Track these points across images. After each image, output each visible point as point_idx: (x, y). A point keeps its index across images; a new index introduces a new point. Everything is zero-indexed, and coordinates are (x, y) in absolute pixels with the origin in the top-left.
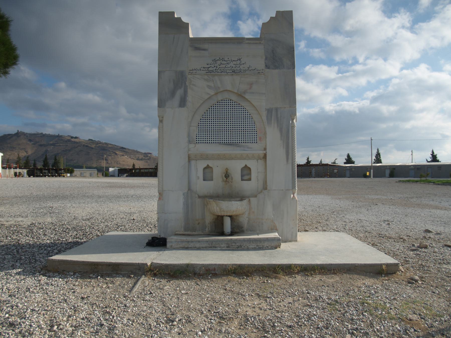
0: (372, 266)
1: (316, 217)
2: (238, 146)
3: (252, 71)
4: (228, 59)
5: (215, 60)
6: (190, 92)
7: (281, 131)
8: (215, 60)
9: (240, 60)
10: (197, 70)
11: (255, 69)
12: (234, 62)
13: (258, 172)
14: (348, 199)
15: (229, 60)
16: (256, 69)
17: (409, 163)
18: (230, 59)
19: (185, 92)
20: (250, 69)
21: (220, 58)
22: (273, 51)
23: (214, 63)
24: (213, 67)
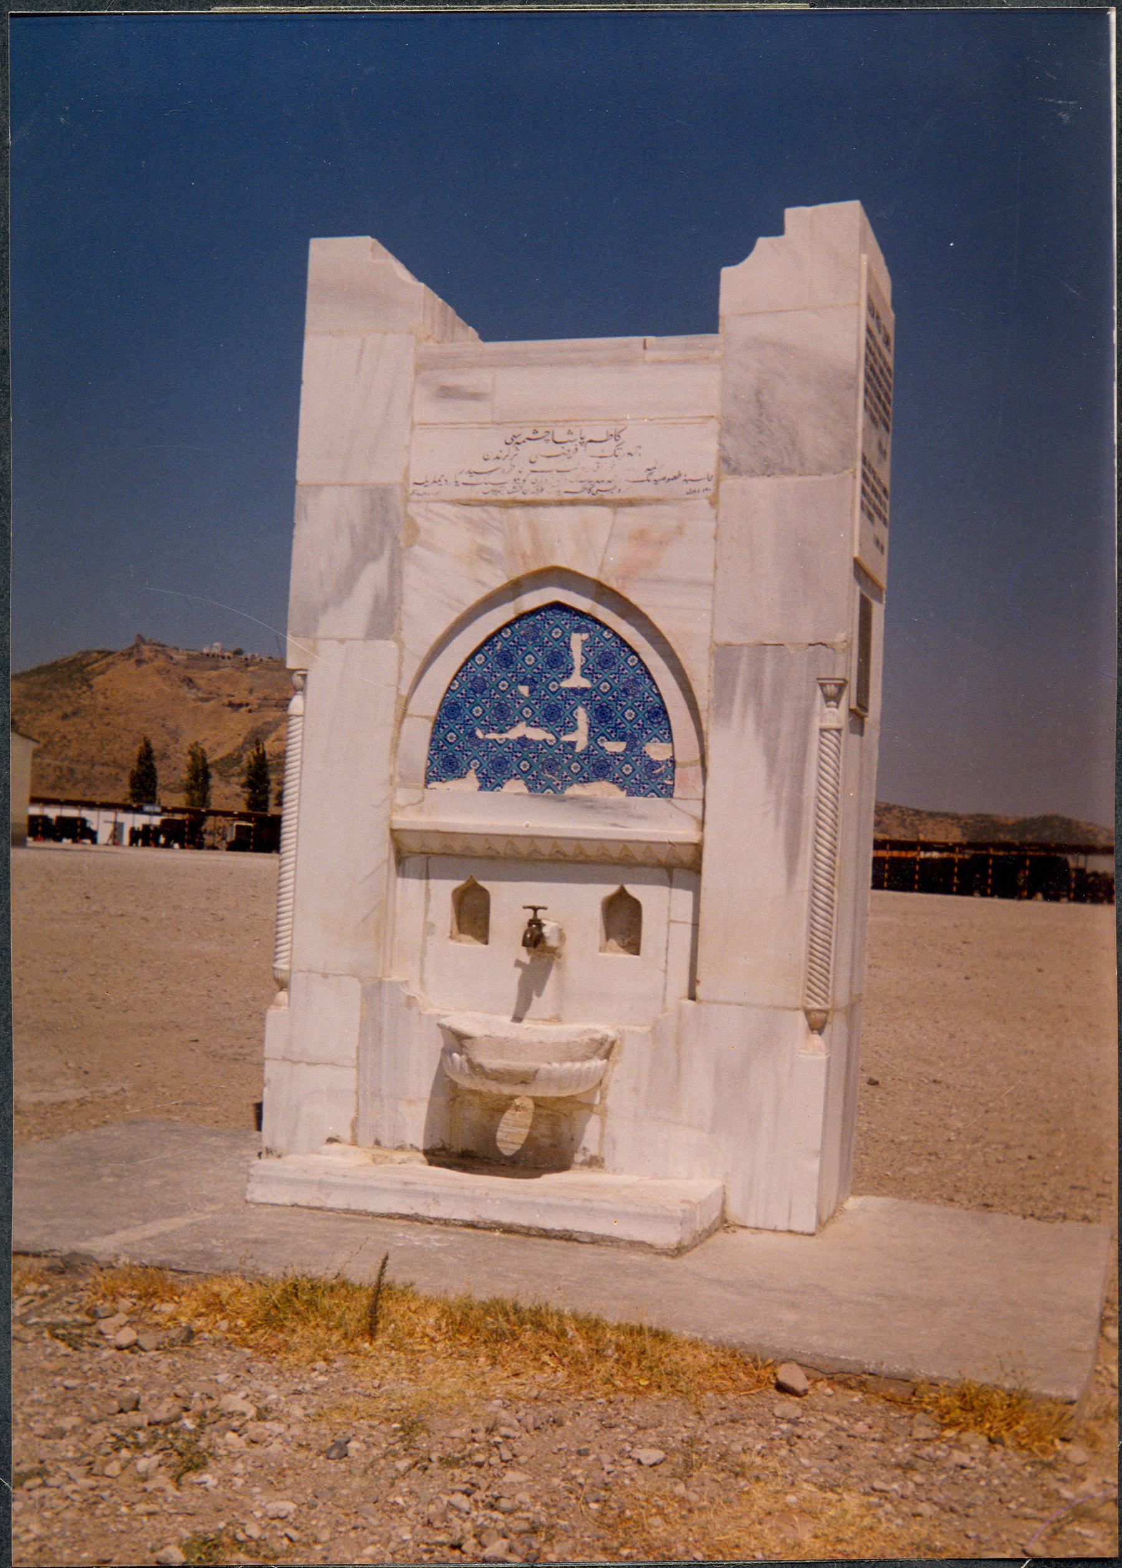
0: (390, 20)
1: (229, 1500)
2: (591, 807)
3: (663, 482)
4: (570, 432)
5: (516, 440)
6: (412, 575)
7: (771, 754)
8: (516, 440)
9: (617, 436)
10: (443, 482)
11: (675, 478)
12: (596, 449)
13: (670, 921)
14: (63, 1272)
15: (571, 438)
16: (682, 478)
17: (591, 1212)
18: (576, 435)
19: (395, 574)
20: (657, 475)
21: (536, 432)
22: (758, 393)
23: (511, 455)
24: (507, 468)
